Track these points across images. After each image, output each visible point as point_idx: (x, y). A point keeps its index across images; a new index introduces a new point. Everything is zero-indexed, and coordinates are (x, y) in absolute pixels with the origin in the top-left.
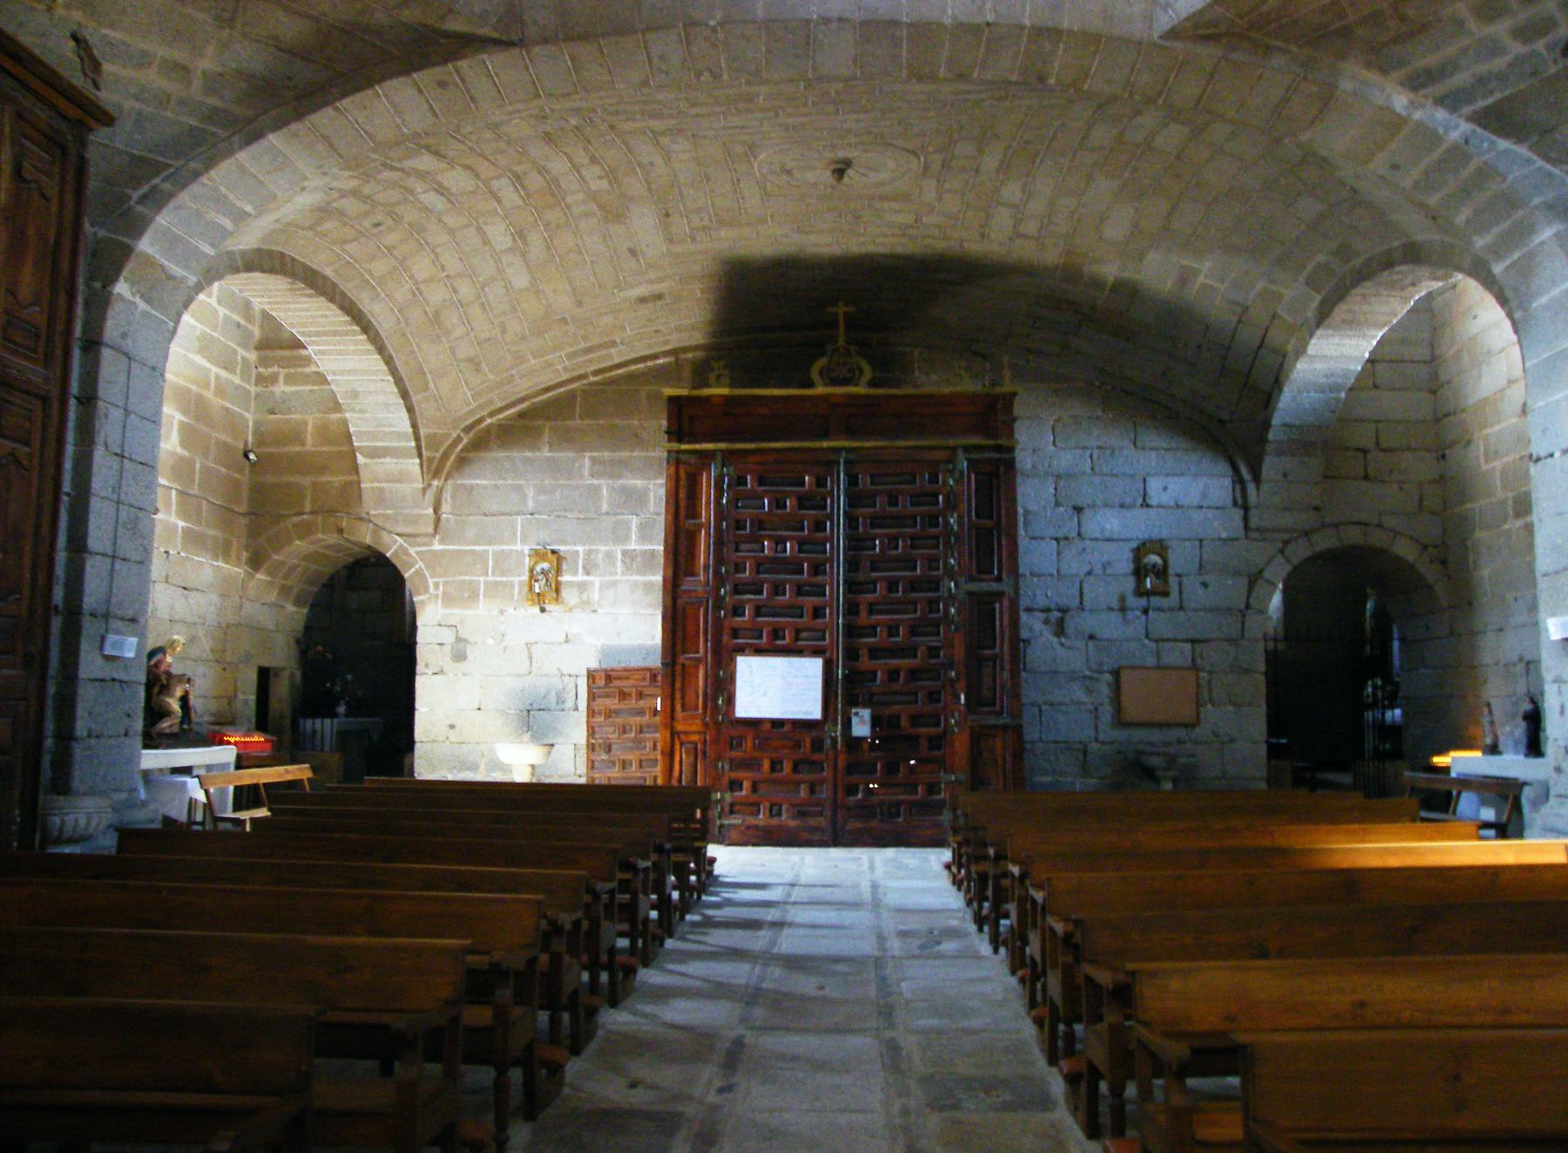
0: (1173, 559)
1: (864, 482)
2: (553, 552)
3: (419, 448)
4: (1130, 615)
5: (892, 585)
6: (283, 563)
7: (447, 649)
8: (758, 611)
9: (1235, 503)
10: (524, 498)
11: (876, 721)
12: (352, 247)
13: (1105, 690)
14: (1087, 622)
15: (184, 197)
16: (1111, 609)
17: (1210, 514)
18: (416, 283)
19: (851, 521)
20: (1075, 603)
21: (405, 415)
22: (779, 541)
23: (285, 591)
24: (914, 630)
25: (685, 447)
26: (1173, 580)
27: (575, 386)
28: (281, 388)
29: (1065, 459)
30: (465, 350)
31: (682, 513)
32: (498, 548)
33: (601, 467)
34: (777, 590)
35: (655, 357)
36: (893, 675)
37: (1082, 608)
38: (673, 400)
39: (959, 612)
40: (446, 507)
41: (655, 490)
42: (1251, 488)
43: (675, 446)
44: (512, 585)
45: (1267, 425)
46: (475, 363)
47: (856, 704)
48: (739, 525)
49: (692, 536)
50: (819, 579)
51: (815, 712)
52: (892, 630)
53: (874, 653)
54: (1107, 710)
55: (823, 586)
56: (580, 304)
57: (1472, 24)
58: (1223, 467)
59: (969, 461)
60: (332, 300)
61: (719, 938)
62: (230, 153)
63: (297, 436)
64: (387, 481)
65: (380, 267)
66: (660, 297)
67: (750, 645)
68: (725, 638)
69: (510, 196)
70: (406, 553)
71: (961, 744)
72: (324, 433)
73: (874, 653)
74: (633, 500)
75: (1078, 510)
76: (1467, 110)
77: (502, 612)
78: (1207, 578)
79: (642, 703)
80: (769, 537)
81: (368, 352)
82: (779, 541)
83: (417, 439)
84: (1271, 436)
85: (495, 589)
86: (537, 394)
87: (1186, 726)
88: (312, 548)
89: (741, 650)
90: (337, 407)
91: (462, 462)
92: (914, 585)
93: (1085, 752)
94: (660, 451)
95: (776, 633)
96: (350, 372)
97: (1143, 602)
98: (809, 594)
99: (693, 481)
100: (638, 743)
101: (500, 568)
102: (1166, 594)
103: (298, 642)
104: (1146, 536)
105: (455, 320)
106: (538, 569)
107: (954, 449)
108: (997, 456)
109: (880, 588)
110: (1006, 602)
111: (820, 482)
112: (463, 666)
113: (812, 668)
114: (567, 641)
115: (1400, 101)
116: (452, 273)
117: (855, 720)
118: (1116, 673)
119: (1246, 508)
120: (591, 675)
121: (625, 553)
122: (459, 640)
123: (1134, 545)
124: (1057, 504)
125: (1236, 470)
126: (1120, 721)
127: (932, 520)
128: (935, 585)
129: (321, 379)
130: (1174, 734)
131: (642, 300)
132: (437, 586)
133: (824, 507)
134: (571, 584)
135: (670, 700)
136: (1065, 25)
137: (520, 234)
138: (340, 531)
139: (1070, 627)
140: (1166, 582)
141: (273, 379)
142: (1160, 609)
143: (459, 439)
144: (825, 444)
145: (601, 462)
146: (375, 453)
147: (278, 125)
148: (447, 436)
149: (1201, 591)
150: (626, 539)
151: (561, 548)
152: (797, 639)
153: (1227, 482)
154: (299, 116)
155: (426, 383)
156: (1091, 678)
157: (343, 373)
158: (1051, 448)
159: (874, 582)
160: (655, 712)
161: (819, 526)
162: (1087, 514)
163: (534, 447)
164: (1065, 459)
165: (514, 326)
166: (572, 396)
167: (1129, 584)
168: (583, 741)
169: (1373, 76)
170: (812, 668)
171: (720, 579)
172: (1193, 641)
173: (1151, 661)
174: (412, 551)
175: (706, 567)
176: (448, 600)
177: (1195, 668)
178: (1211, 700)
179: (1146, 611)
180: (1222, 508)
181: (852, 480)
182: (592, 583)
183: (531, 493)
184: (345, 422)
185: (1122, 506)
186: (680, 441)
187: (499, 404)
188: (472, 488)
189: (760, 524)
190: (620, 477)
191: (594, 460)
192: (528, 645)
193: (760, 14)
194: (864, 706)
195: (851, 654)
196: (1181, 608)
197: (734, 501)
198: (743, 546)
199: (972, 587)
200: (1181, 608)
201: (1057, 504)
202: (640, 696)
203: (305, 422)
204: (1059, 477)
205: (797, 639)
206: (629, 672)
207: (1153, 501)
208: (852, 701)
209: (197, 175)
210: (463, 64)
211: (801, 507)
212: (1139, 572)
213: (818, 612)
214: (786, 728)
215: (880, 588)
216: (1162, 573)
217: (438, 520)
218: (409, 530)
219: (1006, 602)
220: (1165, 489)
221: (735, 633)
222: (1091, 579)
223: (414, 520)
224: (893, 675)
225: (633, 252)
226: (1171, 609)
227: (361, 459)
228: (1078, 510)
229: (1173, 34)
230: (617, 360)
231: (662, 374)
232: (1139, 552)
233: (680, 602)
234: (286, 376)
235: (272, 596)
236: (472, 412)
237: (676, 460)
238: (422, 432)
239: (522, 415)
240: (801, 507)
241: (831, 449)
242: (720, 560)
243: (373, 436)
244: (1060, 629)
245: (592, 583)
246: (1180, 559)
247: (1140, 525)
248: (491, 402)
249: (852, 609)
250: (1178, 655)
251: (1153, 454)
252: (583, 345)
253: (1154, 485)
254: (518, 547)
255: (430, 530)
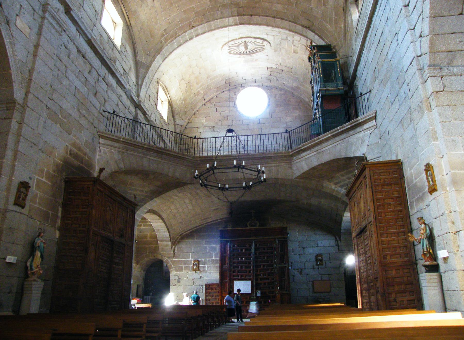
0: (323, 257)
1: (258, 245)
2: (198, 260)
3: (170, 240)
4: (315, 270)
5: (264, 266)
6: (142, 263)
7: (176, 281)
8: (238, 272)
9: (336, 245)
10: (192, 249)
11: (262, 293)
12: (161, 206)
13: (311, 285)
14: (306, 271)
15: (141, 209)
16: (311, 268)
17: (331, 248)
18: (171, 210)
19: (256, 253)
20: (304, 267)
21: (168, 233)
22: (242, 258)
23: (142, 269)
24: (269, 275)
25: (223, 240)
26: (324, 262)
27: (201, 226)
28: (142, 227)
29: (300, 238)
30: (180, 220)
31: (223, 253)
32: (186, 259)
33: (207, 243)
34: (242, 267)
35: (217, 220)
36: (265, 284)
37: (305, 268)
38: (220, 230)
39: (277, 271)
40: (176, 251)
41: (218, 247)
42: (339, 242)
43: (221, 240)
44: (189, 267)
45: (341, 229)
46: (181, 223)
47: (258, 290)
48: (234, 255)
49: (225, 257)
50: (250, 265)
51: (250, 292)
52: (264, 275)
53: (261, 279)
54: (311, 290)
55: (251, 266)
56: (202, 211)
57: (340, 177)
58: (334, 238)
59: (279, 241)
60: (156, 215)
61: (228, 327)
62: (148, 201)
63: (145, 237)
64: (164, 246)
65: (165, 208)
66: (218, 209)
67: (237, 279)
68: (232, 277)
69: (189, 195)
70: (168, 261)
71: (278, 296)
72: (151, 236)
73: (261, 279)
74: (213, 249)
75: (304, 248)
76: (344, 188)
77: (187, 272)
78: (331, 261)
79: (216, 291)
80: (240, 257)
81: (161, 223)
82: (242, 258)
83: (170, 238)
84: (342, 231)
85: (186, 268)
86: (194, 228)
87: (328, 292)
88: (148, 260)
89: (235, 279)
90: (154, 231)
91: (179, 242)
92: (268, 266)
93: (307, 299)
94: (218, 239)
95: (242, 276)
96: (158, 226)
97: (317, 267)
98: (248, 268)
99: (225, 246)
100: (215, 299)
101: (187, 264)
102: (322, 265)
103: (144, 279)
104: (318, 253)
105: (178, 215)
106: (195, 264)
107: (275, 238)
108: (284, 239)
109: (262, 266)
110: (286, 268)
111: (250, 246)
112: (179, 284)
113: (249, 283)
114: (201, 278)
115: (333, 187)
116: (178, 207)
117: (257, 293)
118: (313, 282)
119: (338, 246)
120: (206, 285)
121: (212, 260)
122: (179, 278)
123: (315, 255)
124: (299, 247)
125: (336, 238)
126: (314, 292)
127: (271, 253)
128: (272, 265)
129: (151, 225)
130: (326, 294)
131: (214, 210)
132: (174, 267)
133: (250, 251)
134: (201, 266)
135: (221, 290)
136: (279, 177)
137: (191, 200)
138: (154, 256)
139: (303, 272)
140: (322, 262)
141: (141, 225)
142: (321, 268)
143: (178, 238)
144: (250, 238)
145: (207, 242)
146: (162, 241)
147: (155, 197)
148: (176, 237)
149: (330, 264)
150: (212, 257)
151: (199, 259)
152: (246, 277)
153: (334, 241)
154: (159, 196)
155: (172, 227)
156: (308, 283)
157: (156, 226)
158: (297, 236)
159: (260, 265)
160: (219, 292)
161: (249, 255)
162: (306, 249)
163: (193, 239)
164: (300, 238)
165: (189, 216)
166: (201, 228)
167: (315, 263)
168: (204, 299)
169: (328, 183)
170: (249, 283)
171: (230, 266)
172: (329, 274)
173: (320, 279)
174: (169, 260)
175: (228, 263)
176: (177, 270)
177: (329, 280)
178: (333, 287)
179: (318, 269)
180: (333, 246)
181: (256, 245)
182: (205, 266)
183: (193, 248)
184: (156, 235)
185: (313, 247)
186: (222, 239)
187: (186, 230)
188: (181, 247)
189: (238, 254)
190: (211, 244)
191: (205, 242)
192: (193, 279)
193: (231, 178)
194: (259, 290)
195: (256, 280)
196: (326, 268)
197: (233, 249)
198: (235, 259)
199: (280, 266)
200: (326, 268)
201: (299, 247)
202: (216, 289)
203: (147, 234)
204: (299, 242)
205: (246, 277)
206: (213, 284)
207: (319, 246)
208: (257, 289)
209: (143, 205)
210: (185, 187)
211: (246, 251)
212: (317, 260)
213: (250, 272)
214: (244, 295)
215: (262, 266)
216: (321, 260)
217: (174, 254)
218: (168, 256)
219: (286, 268)
220: (321, 243)
221: (234, 276)
222: (307, 262)
223: (170, 254)
224: (265, 284)
225: (212, 202)
226: (324, 268)
227: (159, 242)
228: (304, 248)
229: (296, 178)
230: (210, 221)
231: (218, 224)
232: (317, 256)
233: (223, 270)
234: (143, 225)
235: (140, 270)
236: (181, 232)
237: (221, 242)
238: (171, 237)
239: (191, 232)
240: (246, 251)
241: (251, 239)
242: (230, 262)
243: (161, 237)
244: (301, 273)
245: (205, 266)
246: (325, 258)
247: (317, 251)
248: (185, 230)
249: (256, 271)
250: (325, 277)
251: (319, 236)
252: (203, 218)
253: (319, 243)
254: (191, 259)
255: (173, 256)
